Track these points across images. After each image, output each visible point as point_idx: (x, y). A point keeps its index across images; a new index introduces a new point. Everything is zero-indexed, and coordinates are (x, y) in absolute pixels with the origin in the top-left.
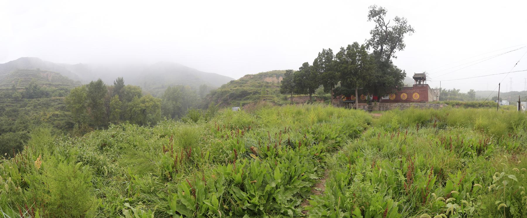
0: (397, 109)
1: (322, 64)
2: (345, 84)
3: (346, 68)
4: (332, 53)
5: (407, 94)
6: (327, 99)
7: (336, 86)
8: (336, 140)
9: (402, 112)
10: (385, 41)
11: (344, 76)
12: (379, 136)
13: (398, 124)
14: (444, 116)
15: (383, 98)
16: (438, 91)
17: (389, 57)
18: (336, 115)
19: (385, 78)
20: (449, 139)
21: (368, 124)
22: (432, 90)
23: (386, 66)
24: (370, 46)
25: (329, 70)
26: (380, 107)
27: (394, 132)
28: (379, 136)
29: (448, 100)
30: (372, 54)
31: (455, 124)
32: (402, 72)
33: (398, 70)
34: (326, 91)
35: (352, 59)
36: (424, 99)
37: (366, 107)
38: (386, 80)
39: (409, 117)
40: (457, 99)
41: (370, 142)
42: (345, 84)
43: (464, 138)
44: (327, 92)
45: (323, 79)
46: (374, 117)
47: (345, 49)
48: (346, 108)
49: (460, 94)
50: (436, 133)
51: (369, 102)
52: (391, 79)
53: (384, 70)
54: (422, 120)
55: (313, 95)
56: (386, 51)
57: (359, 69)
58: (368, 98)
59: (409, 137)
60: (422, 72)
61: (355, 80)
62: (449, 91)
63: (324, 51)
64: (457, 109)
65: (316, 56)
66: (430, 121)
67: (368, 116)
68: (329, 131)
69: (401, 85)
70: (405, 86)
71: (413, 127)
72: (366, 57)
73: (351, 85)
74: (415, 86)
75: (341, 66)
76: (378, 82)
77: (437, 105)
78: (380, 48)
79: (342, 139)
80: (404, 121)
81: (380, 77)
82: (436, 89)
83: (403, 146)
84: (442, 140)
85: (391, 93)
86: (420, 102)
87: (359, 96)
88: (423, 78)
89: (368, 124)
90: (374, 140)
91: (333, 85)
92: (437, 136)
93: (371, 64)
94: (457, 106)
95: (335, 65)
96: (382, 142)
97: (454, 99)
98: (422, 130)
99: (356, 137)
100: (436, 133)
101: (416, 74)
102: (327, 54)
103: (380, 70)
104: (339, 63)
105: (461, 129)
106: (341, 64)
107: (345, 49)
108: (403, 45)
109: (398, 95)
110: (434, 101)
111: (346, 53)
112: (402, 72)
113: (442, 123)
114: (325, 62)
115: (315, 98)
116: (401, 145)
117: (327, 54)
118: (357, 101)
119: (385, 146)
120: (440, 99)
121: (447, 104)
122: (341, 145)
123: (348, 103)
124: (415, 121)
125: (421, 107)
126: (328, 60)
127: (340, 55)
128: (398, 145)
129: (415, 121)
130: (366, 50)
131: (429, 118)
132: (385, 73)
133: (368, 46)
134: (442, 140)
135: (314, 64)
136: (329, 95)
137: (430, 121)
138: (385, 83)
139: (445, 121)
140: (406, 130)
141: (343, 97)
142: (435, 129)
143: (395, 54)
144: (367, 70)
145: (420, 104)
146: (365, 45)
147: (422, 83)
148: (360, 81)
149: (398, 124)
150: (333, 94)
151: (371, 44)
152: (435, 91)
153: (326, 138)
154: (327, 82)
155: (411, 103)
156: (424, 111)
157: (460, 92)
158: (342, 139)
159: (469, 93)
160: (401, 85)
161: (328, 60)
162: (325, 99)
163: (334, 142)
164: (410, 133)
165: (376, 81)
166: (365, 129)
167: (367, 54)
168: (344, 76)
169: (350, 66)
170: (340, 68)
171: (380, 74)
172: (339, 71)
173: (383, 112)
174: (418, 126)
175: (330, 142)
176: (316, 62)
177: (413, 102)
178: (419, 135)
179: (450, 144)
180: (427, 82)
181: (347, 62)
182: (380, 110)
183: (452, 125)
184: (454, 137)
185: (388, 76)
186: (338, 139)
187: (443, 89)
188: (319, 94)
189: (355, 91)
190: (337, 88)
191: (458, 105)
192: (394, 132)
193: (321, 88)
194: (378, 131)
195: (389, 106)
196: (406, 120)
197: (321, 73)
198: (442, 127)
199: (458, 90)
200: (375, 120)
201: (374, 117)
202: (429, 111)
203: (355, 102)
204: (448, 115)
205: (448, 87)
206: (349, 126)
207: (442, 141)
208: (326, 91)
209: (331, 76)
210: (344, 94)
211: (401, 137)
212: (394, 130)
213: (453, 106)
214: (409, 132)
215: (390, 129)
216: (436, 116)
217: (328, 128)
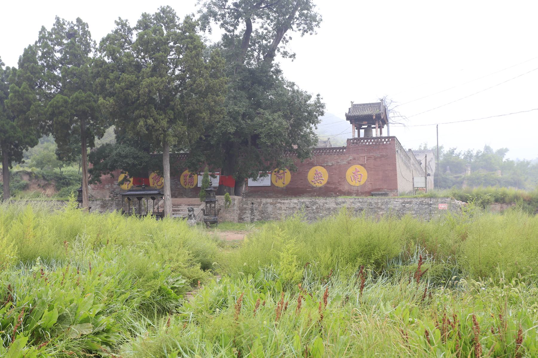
0: (296, 219)
1: (52, 67)
2: (130, 135)
3: (132, 85)
4: (86, 33)
5: (328, 168)
6: (68, 184)
7: (98, 142)
8: (95, 325)
9: (312, 226)
10: (258, 6)
11: (125, 111)
12: (238, 308)
13: (299, 267)
14: (450, 242)
15: (251, 183)
16: (430, 156)
17: (270, 56)
18: (88, 236)
19: (257, 120)
20: (469, 323)
21: (205, 267)
22: (409, 154)
23: (260, 83)
24: (211, 19)
25: (78, 88)
26: (242, 210)
27: (288, 294)
28: (238, 308)
29: (465, 187)
30: (217, 46)
31: (492, 269)
32: (311, 101)
33: (297, 94)
34: (64, 155)
35: (156, 59)
36: (383, 185)
37: (198, 211)
38: (261, 125)
39: (335, 245)
40: (499, 182)
41: (208, 329)
42: (130, 135)
43: (526, 323)
44: (70, 161)
45: (52, 116)
46: (221, 245)
47: (133, 24)
48: (127, 213)
49: (509, 165)
50: (425, 299)
51: (207, 194)
52: (278, 122)
53: (254, 95)
54: (377, 255)
55: (16, 168)
56: (263, 37)
57: (176, 89)
58: (205, 181)
59: (335, 311)
60: (373, 99)
61: (164, 123)
62: (469, 155)
63: (59, 24)
64: (499, 219)
65: (32, 39)
66: (405, 259)
67: (202, 238)
68: (73, 294)
69: (308, 142)
70: (320, 145)
71: (348, 277)
72: (198, 55)
73: (149, 142)
74: (353, 143)
75: (117, 78)
76: (236, 134)
77: (426, 203)
78: (242, 26)
79: (118, 318)
80: (316, 257)
81: (244, 116)
82: (424, 151)
83: (316, 340)
84: (446, 326)
85: (278, 165)
86: (370, 194)
87: (175, 174)
88: (378, 117)
89: (205, 267)
90: (223, 321)
91: (87, 138)
92: (428, 310)
93: (214, 76)
94: (498, 206)
95: (98, 75)
96: (247, 328)
97: (487, 182)
98: (378, 290)
99: (164, 311)
100: (425, 299)
101: (355, 107)
102: (71, 37)
103: (243, 93)
104: (110, 69)
105: (515, 291)
106: (117, 73)
107: (133, 24)
108: (313, 18)
109: (298, 173)
110: (416, 190)
111: (134, 38)
112: (311, 101)
113: (444, 268)
114: (61, 61)
115: (25, 180)
116: (308, 338)
117: (71, 35)
118: (168, 192)
119: (257, 343)
120: (437, 184)
121: (464, 199)
122: (113, 340)
123: (135, 201)
124: (352, 259)
125: (374, 210)
126: (74, 55)
127: (112, 43)
128: (297, 338)
129: (352, 259)
130: (199, 33)
131: (399, 250)
132: (258, 105)
133: (205, 20)
134: (446, 326)
135: (22, 63)
136: (73, 169)
137: (405, 259)
138: (256, 137)
139: (454, 261)
140: (322, 288)
141: (122, 177)
142: (422, 287)
143: (290, 47)
144: (203, 95)
145: (369, 199)
146: (197, 16)
147: (375, 133)
148: (181, 128)
149: (299, 267)
150: (90, 166)
151: (215, 15)
152: (421, 158)
153: (61, 319)
154: (68, 127)
155: (340, 199)
156: (380, 227)
157: (509, 157)
158: (118, 318)
159: (527, 161)
160: (306, 140)
161: (74, 55)
162: (62, 183)
163: (87, 330)
164: (338, 297)
165: (232, 129)
166: (195, 283)
167: (202, 47)
168: (125, 111)
169: (146, 81)
170: (111, 83)
171: (241, 107)
172: (112, 94)
173: (253, 228)
174: (363, 276)
175: (76, 331)
176: (28, 57)
177: (349, 193)
178: (366, 305)
179: (473, 342)
180: (391, 130)
181: (138, 67)
182: (241, 219)
183: (481, 275)
184: (485, 317)
185: (267, 114)
186: (105, 321)
187: (446, 150)
188: (40, 164)
189: (160, 159)
190: (104, 147)
191: (501, 200)
192: (288, 294)
193: (47, 146)
194: (234, 290)
195: (270, 209)
196: (325, 256)
197: (49, 97)
198: (446, 278)
199: (502, 152)
200: (226, 253)
201: (221, 245)
202: (400, 225)
203: (161, 195)
204: (464, 238)
205: (464, 140)
206: (141, 275)
207: (443, 331)
208: (64, 155)
209: (80, 107)
210: (125, 169)
211: (309, 312)
212: (287, 286)
213: (484, 204)
214: (334, 292)
215: (273, 284)
216: (423, 241)
217: (68, 283)
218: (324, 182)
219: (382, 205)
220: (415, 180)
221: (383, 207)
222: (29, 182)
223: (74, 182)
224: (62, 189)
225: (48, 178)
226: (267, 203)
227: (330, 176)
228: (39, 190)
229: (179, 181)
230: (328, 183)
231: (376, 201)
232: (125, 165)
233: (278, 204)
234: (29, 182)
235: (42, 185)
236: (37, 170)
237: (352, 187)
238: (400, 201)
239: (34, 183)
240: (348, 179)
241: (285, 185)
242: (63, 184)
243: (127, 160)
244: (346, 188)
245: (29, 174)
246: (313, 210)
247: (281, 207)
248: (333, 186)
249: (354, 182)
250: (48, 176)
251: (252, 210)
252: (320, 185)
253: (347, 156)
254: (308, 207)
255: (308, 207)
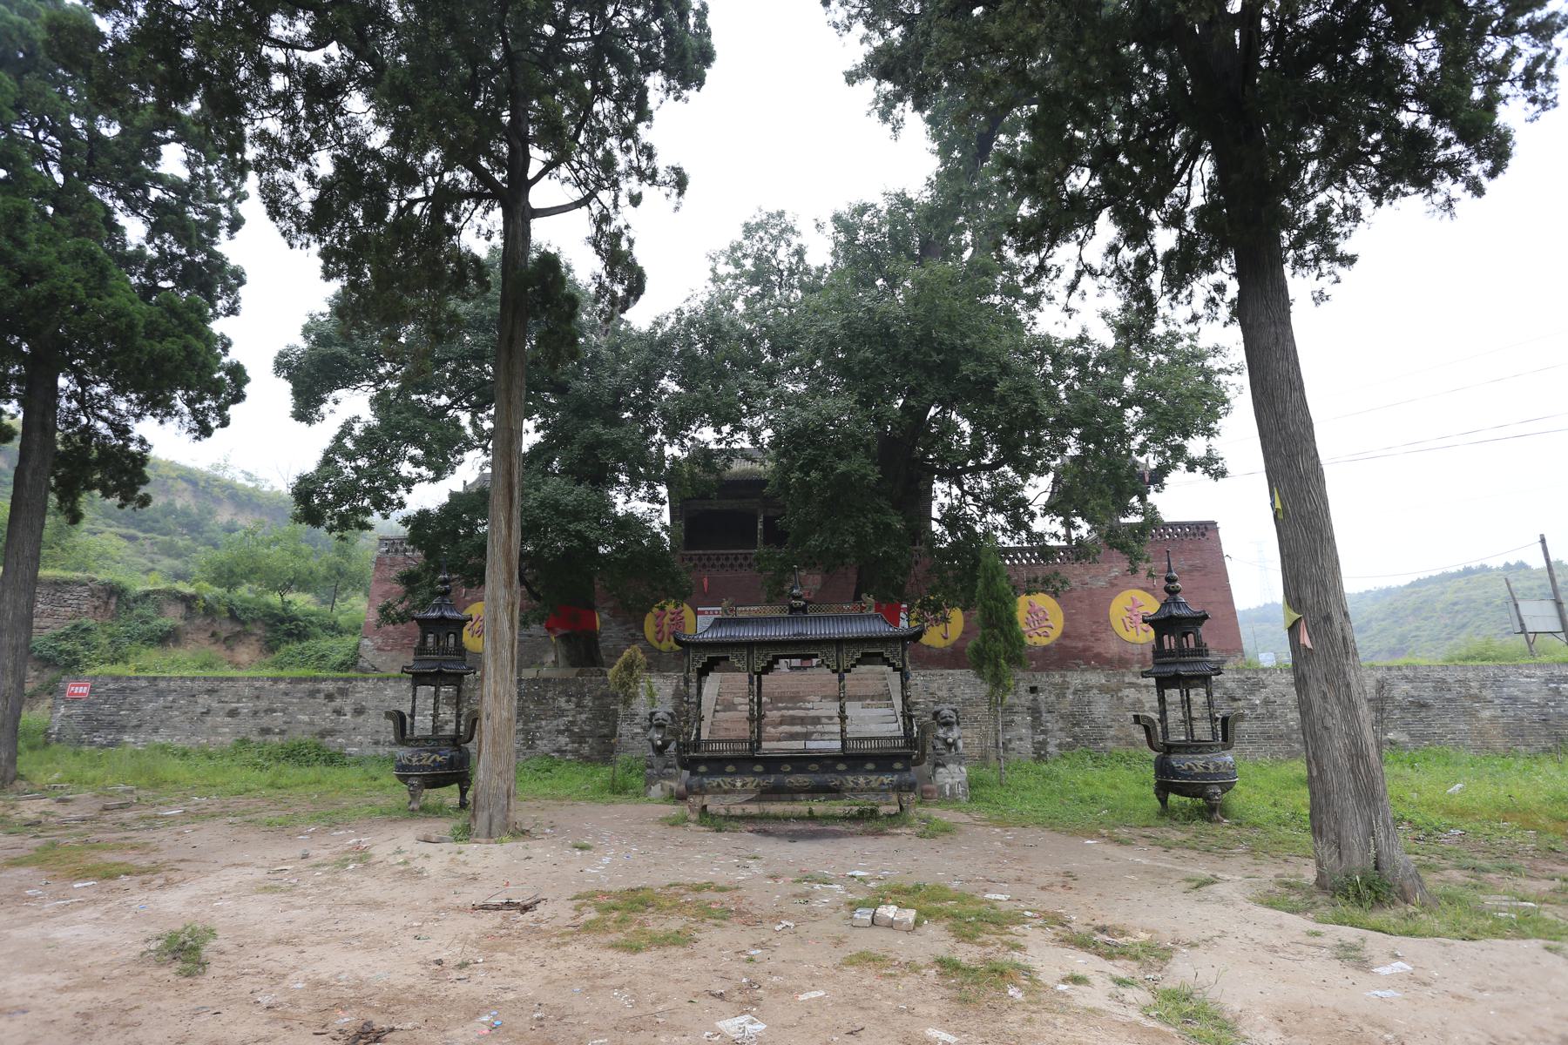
115: (172, 617)
218: (1055, 634)
219: (1483, 686)
220: (1523, 612)
221: (1488, 694)
222: (181, 623)
223: (319, 630)
224: (284, 649)
225: (244, 617)
226: (1088, 688)
227: (1068, 618)
228: (214, 648)
229: (641, 628)
230: (1065, 635)
231: (1460, 676)
232: (576, 543)
233: (1126, 692)
234: (181, 623)
235: (224, 635)
236: (211, 592)
237: (1129, 647)
238: (1538, 673)
239: (199, 629)
240: (1118, 626)
241: (948, 642)
242: (289, 634)
243: (581, 527)
244: (1113, 649)
245: (188, 601)
246: (1253, 707)
247: (1139, 701)
248: (1080, 645)
249: (1133, 631)
250: (245, 610)
251: (1035, 711)
252: (1045, 642)
253: (1106, 566)
254: (1234, 700)
255: (1234, 700)
